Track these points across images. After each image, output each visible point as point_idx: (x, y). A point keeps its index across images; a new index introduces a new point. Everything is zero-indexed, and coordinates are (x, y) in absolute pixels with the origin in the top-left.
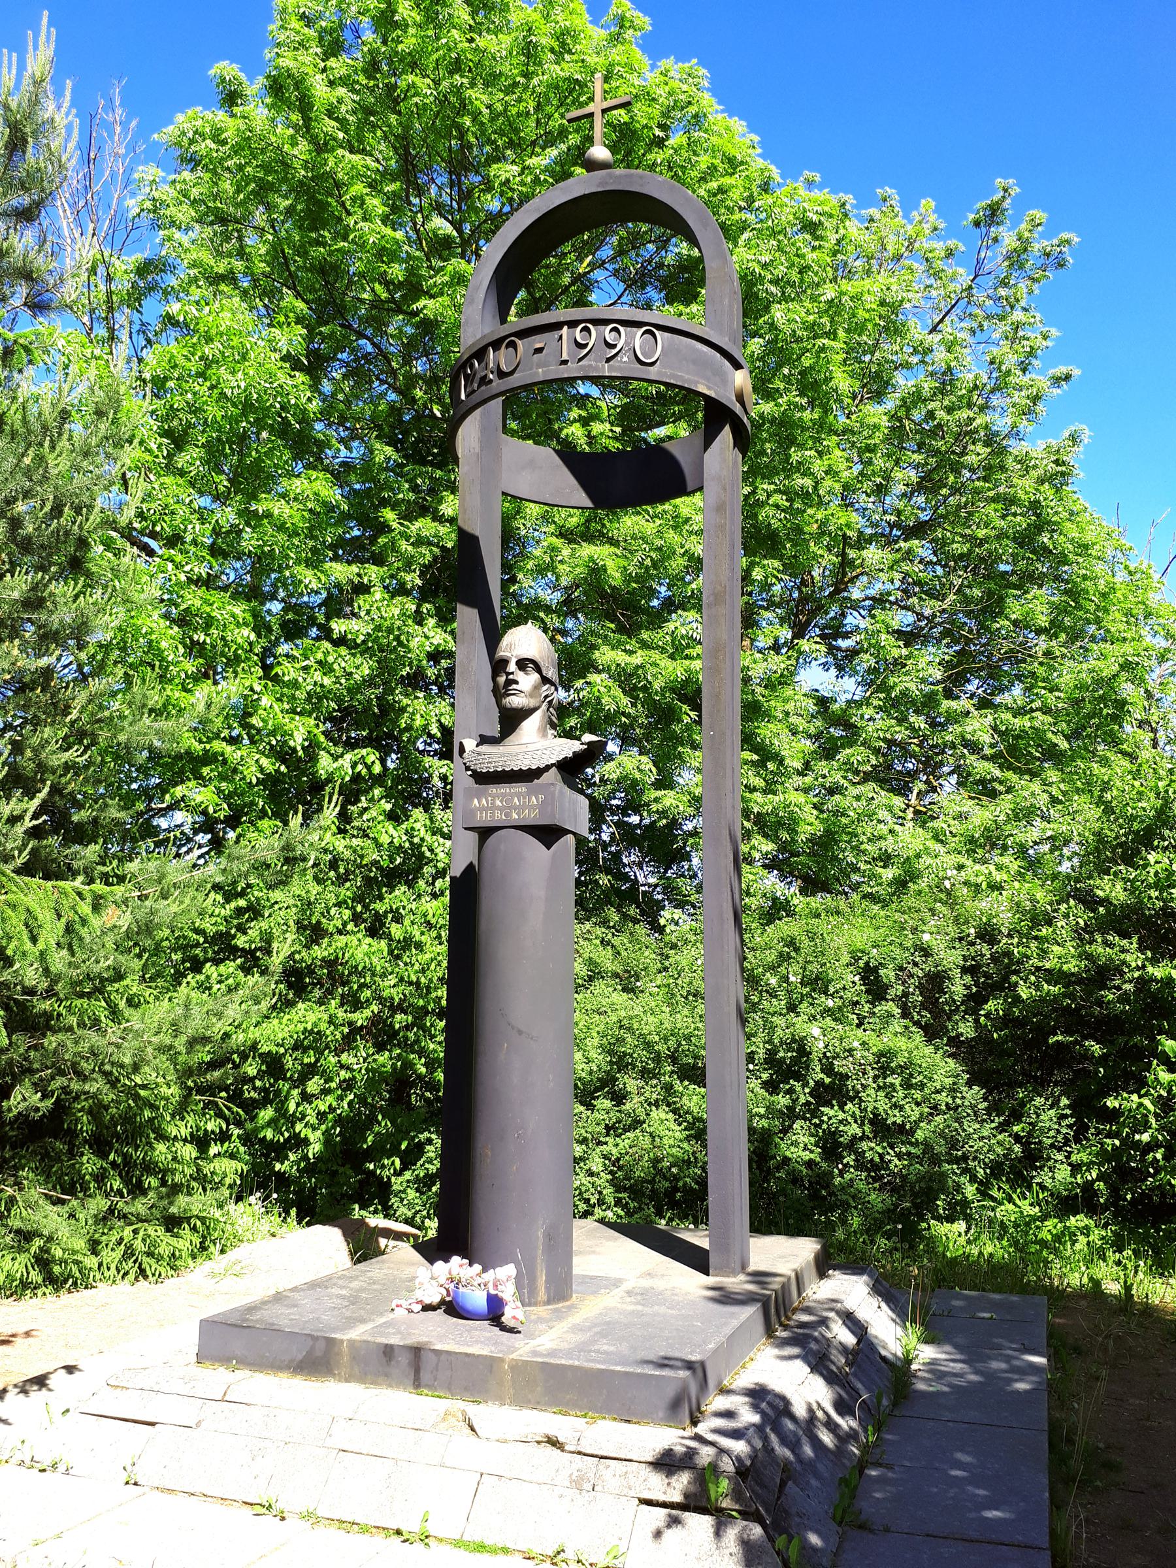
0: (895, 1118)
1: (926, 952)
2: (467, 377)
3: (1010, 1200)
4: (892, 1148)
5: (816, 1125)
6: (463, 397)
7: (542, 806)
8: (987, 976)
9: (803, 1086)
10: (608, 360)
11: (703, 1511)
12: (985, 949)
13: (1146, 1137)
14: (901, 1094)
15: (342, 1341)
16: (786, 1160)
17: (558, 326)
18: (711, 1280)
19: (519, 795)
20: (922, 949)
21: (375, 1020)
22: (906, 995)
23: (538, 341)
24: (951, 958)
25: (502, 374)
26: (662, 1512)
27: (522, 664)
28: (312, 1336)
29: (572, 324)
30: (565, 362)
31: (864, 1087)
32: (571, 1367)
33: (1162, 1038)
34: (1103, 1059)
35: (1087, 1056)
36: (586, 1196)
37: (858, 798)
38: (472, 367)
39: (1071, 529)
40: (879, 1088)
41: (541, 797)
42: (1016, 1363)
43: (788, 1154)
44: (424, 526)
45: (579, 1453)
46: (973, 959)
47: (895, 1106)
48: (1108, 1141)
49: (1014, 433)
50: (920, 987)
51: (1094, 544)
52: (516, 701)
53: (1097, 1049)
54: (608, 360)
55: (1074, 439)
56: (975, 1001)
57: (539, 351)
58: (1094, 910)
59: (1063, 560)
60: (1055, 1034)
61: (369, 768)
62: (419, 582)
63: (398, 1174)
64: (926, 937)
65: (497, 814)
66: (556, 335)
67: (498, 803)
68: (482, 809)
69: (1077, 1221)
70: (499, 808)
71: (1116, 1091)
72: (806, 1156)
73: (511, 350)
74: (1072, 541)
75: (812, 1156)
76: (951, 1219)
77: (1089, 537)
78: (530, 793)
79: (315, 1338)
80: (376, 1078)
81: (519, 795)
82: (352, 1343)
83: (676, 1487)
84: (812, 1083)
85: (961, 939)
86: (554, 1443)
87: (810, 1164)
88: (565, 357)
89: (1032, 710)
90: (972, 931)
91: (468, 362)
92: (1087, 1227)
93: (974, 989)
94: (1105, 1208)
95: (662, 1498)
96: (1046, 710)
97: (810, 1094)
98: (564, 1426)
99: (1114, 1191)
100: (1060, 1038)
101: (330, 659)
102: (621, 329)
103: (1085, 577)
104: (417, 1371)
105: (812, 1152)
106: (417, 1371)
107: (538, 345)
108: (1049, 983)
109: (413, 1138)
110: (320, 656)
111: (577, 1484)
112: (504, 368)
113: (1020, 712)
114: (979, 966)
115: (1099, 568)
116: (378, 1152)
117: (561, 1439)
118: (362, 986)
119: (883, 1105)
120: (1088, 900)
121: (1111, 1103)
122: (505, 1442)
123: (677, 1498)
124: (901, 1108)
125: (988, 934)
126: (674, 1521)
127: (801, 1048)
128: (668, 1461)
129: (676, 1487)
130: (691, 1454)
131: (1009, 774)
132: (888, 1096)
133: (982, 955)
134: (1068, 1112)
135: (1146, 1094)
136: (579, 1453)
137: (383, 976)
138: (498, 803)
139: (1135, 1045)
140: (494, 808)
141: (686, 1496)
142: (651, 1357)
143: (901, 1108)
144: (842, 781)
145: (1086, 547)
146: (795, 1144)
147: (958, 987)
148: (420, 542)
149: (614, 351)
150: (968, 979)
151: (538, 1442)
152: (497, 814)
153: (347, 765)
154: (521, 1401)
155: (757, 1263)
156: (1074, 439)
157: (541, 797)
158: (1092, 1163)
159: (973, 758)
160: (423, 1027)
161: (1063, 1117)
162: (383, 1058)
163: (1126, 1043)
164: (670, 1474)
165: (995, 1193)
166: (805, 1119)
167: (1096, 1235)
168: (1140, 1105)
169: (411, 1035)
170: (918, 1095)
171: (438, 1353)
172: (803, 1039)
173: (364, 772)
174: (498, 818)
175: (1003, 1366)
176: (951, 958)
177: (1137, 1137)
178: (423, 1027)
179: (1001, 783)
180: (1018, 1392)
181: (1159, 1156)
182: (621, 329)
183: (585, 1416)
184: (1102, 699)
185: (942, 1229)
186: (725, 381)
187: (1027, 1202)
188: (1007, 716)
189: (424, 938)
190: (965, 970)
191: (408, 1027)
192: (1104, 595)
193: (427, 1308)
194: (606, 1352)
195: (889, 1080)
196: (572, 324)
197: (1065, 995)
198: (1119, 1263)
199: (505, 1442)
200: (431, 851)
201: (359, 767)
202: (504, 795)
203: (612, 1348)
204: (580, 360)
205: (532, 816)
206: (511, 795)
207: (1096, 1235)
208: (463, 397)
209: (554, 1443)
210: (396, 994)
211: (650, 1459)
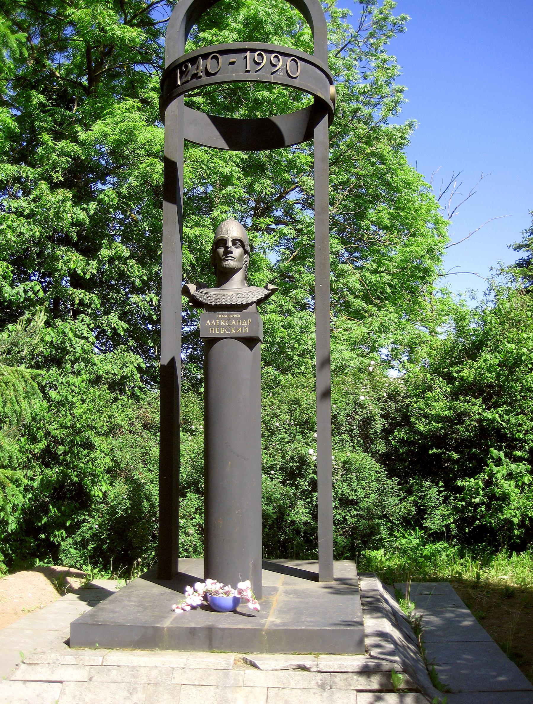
0: (353, 496)
1: (362, 406)
2: (182, 73)
3: (404, 537)
4: (350, 513)
5: (309, 503)
6: (179, 83)
7: (250, 326)
8: (394, 418)
9: (304, 482)
10: (273, 73)
11: (391, 691)
12: (392, 404)
13: (477, 500)
14: (355, 484)
15: (163, 628)
16: (294, 522)
17: (244, 51)
18: (320, 584)
19: (235, 319)
20: (360, 405)
21: (47, 451)
22: (351, 430)
23: (232, 58)
24: (375, 409)
25: (208, 74)
26: (370, 694)
27: (235, 242)
28: (144, 627)
29: (253, 51)
30: (248, 72)
31: (337, 480)
32: (301, 630)
33: (492, 449)
34: (457, 462)
35: (449, 459)
36: (186, 547)
37: (301, 318)
38: (186, 67)
39: (401, 175)
40: (344, 481)
41: (250, 321)
42: (458, 613)
43: (294, 519)
44: (65, 145)
45: (319, 672)
46: (386, 410)
47: (352, 490)
48: (459, 503)
49: (384, 120)
50: (360, 426)
51: (413, 183)
52: (231, 264)
53: (456, 456)
54: (273, 73)
55: (410, 125)
56: (387, 432)
57: (233, 63)
58: (453, 384)
59: (396, 190)
60: (432, 449)
61: (36, 293)
62: (61, 178)
63: (63, 540)
64: (362, 398)
65: (222, 330)
66: (243, 55)
67: (222, 323)
68: (212, 326)
69: (439, 545)
70: (223, 326)
71: (463, 478)
72: (304, 519)
73: (214, 60)
74: (401, 180)
75: (307, 519)
76: (377, 549)
77: (410, 179)
78: (242, 319)
79: (146, 628)
80: (46, 484)
81: (235, 319)
82: (169, 628)
83: (375, 683)
84: (309, 480)
85: (379, 399)
86: (303, 668)
87: (305, 523)
88: (248, 69)
89: (380, 272)
90: (385, 394)
91: (185, 63)
92: (445, 547)
93: (387, 426)
94: (454, 537)
95: (369, 688)
96: (388, 272)
97: (309, 485)
98: (307, 660)
99: (460, 528)
100: (435, 451)
101: (15, 224)
102: (280, 57)
103: (408, 201)
104: (210, 640)
105: (306, 517)
106: (210, 640)
107: (232, 60)
108: (436, 423)
109: (73, 520)
110: (9, 223)
111: (322, 687)
112: (209, 70)
113: (375, 272)
114: (389, 413)
115: (416, 196)
116: (48, 529)
117: (307, 666)
118: (38, 428)
119: (346, 490)
120: (449, 378)
121: (459, 483)
122: (277, 670)
123: (376, 686)
124: (355, 491)
125: (393, 396)
126: (379, 699)
127: (303, 461)
128: (367, 670)
129: (375, 683)
130: (378, 666)
131: (370, 307)
132: (349, 485)
133: (391, 408)
134: (442, 489)
135: (478, 478)
136: (319, 672)
137: (50, 422)
138: (222, 323)
139: (474, 453)
140: (220, 326)
141: (381, 685)
142: (336, 622)
143: (355, 491)
144: (293, 309)
145: (409, 184)
146: (297, 513)
147: (379, 424)
148: (63, 154)
149: (276, 69)
150: (384, 421)
151: (294, 669)
152: (222, 330)
153: (21, 291)
154: (272, 650)
155: (337, 574)
156: (410, 125)
157: (250, 321)
158: (451, 514)
159: (352, 297)
160: (73, 453)
161: (440, 492)
162: (48, 472)
163: (469, 452)
164: (369, 677)
165: (396, 533)
166: (301, 499)
167: (451, 551)
168: (477, 483)
169: (68, 458)
170: (363, 483)
171: (221, 629)
172: (303, 456)
173: (33, 296)
174: (223, 332)
175: (452, 615)
176: (375, 409)
177: (473, 500)
178: (73, 453)
179: (366, 312)
180: (466, 627)
181: (483, 509)
182: (280, 57)
183: (310, 654)
184: (417, 267)
185: (373, 554)
186: (328, 91)
187: (413, 537)
188: (368, 274)
189: (74, 400)
190: (382, 416)
191: (65, 453)
192: (416, 211)
193: (193, 608)
194: (310, 622)
195: (349, 476)
196: (253, 51)
197: (442, 428)
198: (461, 564)
199: (277, 670)
200: (71, 345)
201: (30, 293)
202: (225, 319)
203: (312, 619)
204: (257, 71)
205: (245, 332)
206: (230, 318)
207: (451, 551)
208: (179, 83)
209: (303, 668)
210: (59, 433)
211: (357, 670)
